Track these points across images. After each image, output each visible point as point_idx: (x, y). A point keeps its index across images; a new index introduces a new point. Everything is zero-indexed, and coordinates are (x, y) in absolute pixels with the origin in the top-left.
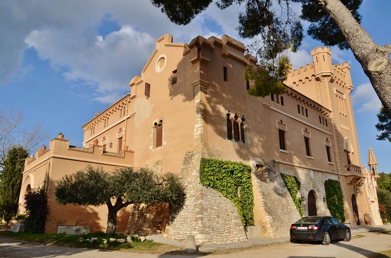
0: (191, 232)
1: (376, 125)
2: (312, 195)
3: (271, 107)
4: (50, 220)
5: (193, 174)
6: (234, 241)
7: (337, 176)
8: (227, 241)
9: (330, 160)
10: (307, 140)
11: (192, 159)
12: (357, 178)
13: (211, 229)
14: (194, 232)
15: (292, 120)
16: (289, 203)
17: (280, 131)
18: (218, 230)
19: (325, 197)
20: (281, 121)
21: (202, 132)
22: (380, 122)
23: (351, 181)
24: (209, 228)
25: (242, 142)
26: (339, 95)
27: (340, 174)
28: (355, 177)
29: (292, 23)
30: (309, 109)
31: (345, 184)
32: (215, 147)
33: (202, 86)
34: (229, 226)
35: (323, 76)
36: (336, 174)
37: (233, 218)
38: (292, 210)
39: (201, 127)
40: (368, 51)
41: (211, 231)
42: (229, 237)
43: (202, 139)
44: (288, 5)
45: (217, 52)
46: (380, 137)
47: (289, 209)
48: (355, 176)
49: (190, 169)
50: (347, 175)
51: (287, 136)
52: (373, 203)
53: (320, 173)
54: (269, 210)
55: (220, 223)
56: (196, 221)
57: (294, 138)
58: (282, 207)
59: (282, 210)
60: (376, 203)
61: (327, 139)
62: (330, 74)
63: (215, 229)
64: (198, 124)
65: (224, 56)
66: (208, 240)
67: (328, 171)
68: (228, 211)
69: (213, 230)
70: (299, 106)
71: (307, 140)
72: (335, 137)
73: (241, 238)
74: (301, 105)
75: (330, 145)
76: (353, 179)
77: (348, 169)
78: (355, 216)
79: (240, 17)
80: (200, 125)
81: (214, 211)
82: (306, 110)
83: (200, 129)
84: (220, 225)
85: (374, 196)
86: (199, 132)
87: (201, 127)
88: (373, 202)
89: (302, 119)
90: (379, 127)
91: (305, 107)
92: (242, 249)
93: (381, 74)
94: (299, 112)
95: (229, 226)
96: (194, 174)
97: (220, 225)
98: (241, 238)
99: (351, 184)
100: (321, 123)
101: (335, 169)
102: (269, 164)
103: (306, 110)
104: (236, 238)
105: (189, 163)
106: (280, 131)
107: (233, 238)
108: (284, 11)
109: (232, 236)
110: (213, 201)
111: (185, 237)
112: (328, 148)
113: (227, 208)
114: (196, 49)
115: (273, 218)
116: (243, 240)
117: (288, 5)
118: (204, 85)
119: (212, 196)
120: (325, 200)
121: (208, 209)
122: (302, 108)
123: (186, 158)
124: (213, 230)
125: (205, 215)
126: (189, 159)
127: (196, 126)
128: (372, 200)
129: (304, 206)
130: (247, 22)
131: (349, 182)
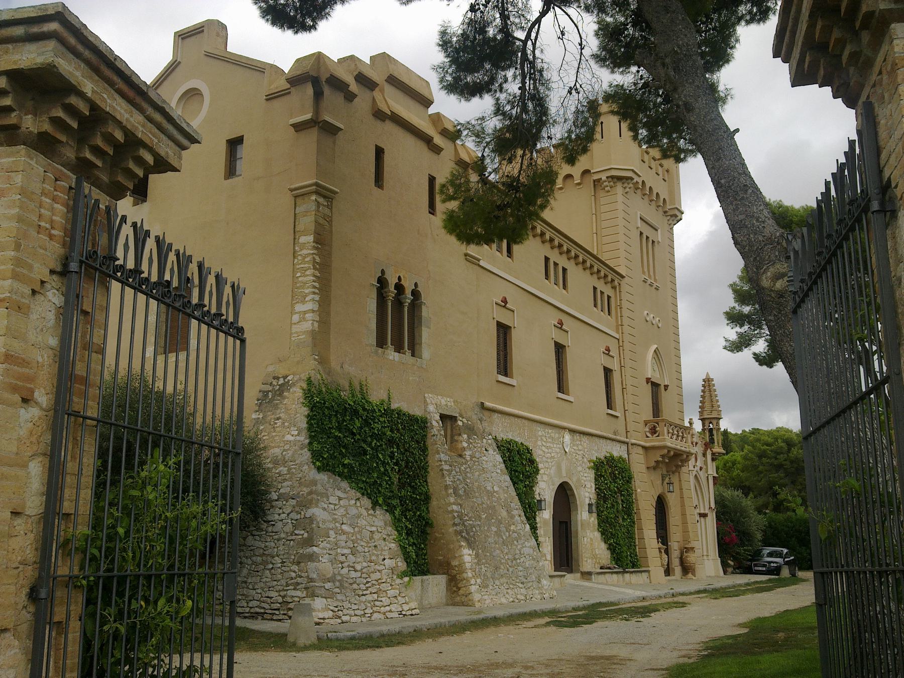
0: (282, 593)
1: (727, 313)
2: (564, 493)
3: (482, 263)
4: (23, 563)
5: (289, 437)
6: (389, 615)
7: (624, 447)
8: (375, 615)
9: (609, 406)
10: (560, 349)
11: (284, 398)
12: (672, 453)
13: (337, 584)
14: (294, 593)
15: (530, 296)
16: (512, 517)
17: (500, 325)
18: (355, 586)
19: (593, 501)
20: (505, 301)
21: (316, 325)
22: (736, 305)
23: (657, 462)
24: (334, 582)
25: (409, 353)
26: (647, 231)
27: (634, 441)
28: (669, 451)
29: (582, 92)
30: (570, 266)
31: (643, 468)
32: (346, 366)
33: (321, 200)
34: (377, 576)
35: (612, 177)
36: (624, 442)
37: (386, 554)
38: (519, 534)
39: (313, 311)
40: (761, 238)
41: (337, 590)
42: (377, 603)
43: (315, 345)
44: (582, 49)
45: (363, 100)
46: (733, 343)
47: (514, 532)
48: (669, 449)
49: (279, 422)
50: (647, 445)
51: (516, 337)
52: (702, 519)
53: (585, 439)
54: (468, 534)
55: (358, 567)
56: (298, 563)
57: (531, 349)
58: (498, 527)
59: (498, 534)
60: (711, 522)
61: (608, 349)
62: (630, 174)
63: (346, 585)
64: (303, 302)
65: (379, 115)
66: (331, 614)
67: (605, 434)
68: (377, 536)
69: (341, 587)
70: (547, 259)
71: (560, 349)
72: (627, 346)
73: (406, 607)
74: (554, 256)
75: (614, 365)
76: (663, 456)
77: (653, 431)
78: (660, 552)
79: (443, 33)
80: (310, 306)
81: (344, 537)
82: (564, 270)
83: (309, 316)
84: (359, 574)
85: (707, 500)
86: (307, 326)
87: (313, 311)
88: (704, 515)
89: (551, 292)
90: (734, 318)
91: (563, 262)
92: (416, 635)
93: (782, 296)
94: (547, 276)
95: (377, 576)
96: (292, 438)
97: (359, 574)
98: (406, 607)
99: (655, 468)
100: (595, 306)
101: (620, 425)
102: (469, 414)
103: (564, 270)
104: (393, 608)
105: (276, 407)
106: (500, 325)
107: (388, 608)
108: (569, 57)
109: (385, 601)
110: (342, 510)
111: (267, 606)
112: (608, 372)
113: (374, 529)
114: (309, 90)
115: (477, 555)
116: (410, 612)
117: (582, 49)
118: (325, 197)
119: (340, 499)
120: (594, 508)
121: (332, 533)
122: (556, 264)
123: (265, 393)
124: (341, 587)
125: (324, 548)
126: (273, 396)
127: (299, 307)
128: (702, 512)
129: (545, 522)
130: (457, 51)
131: (653, 464)
